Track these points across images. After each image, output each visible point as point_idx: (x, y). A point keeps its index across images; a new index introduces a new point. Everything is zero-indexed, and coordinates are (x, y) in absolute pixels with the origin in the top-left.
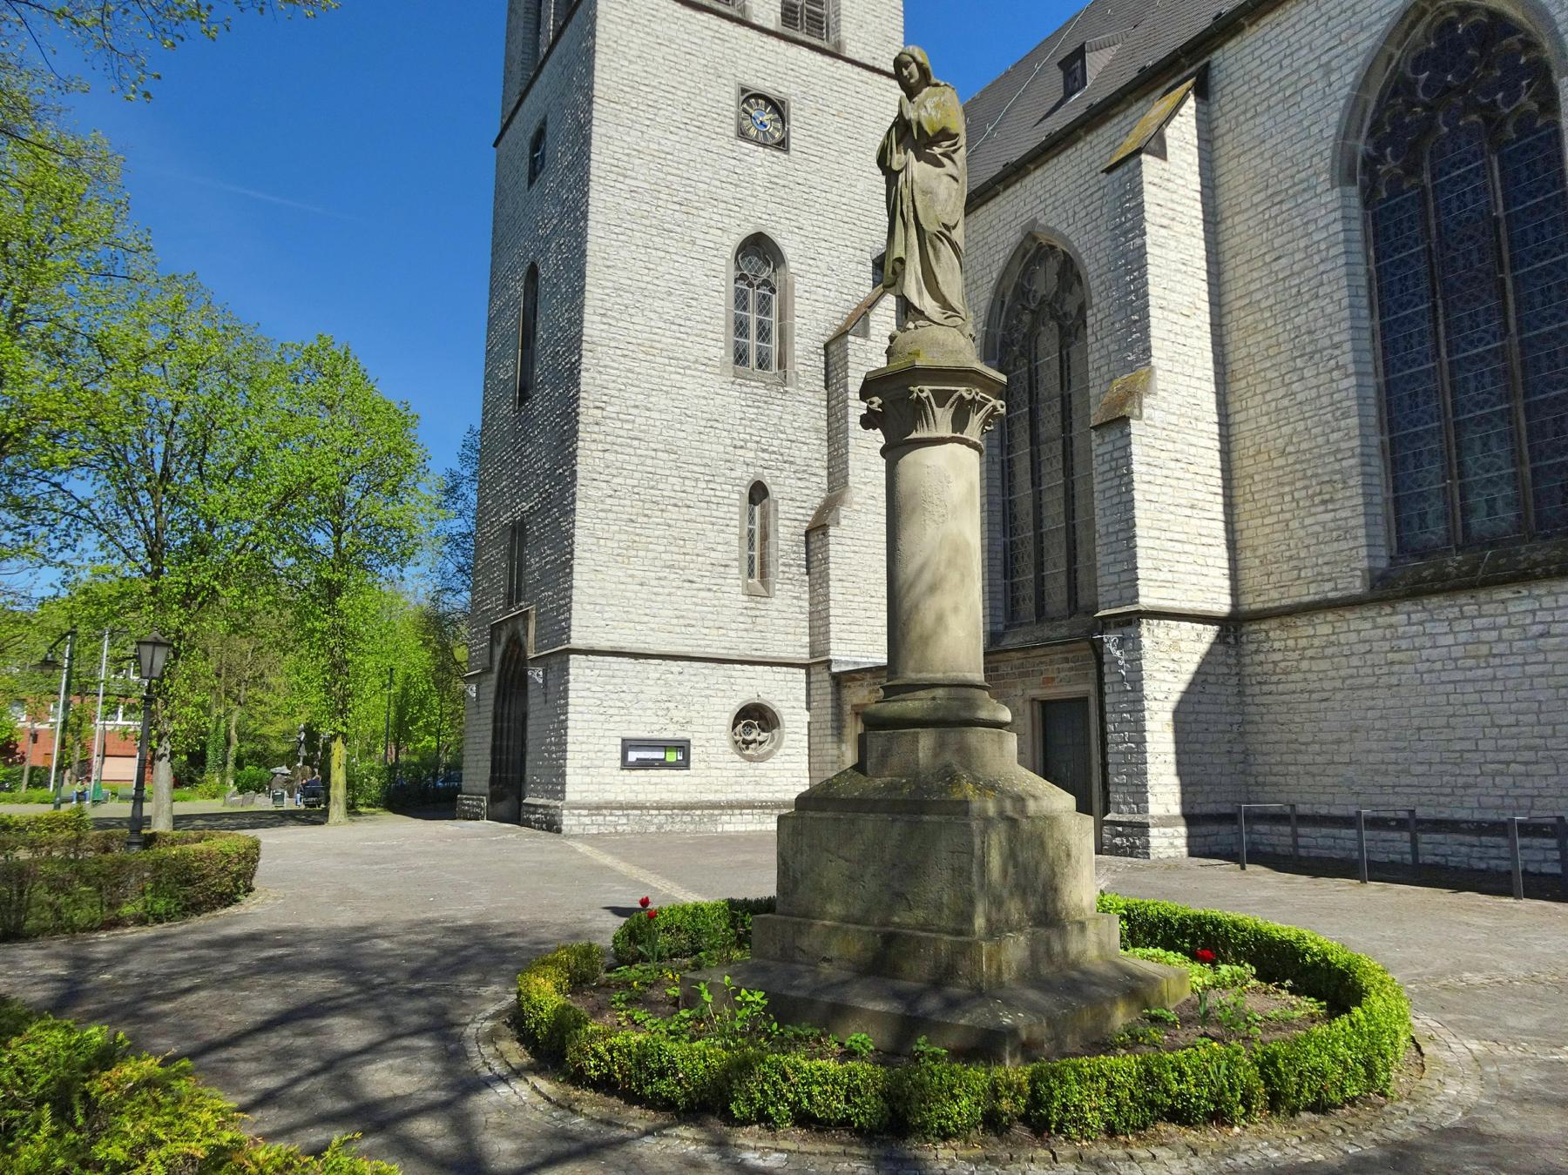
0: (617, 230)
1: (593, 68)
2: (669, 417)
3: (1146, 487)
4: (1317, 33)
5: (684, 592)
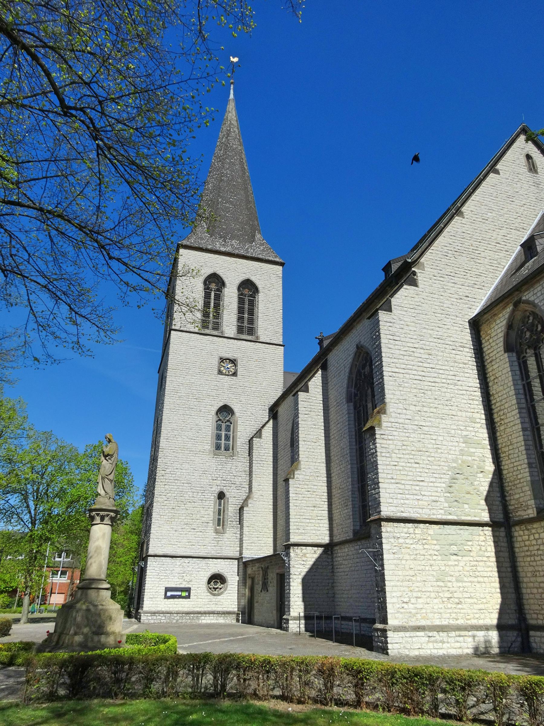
0: (174, 410)
2: (189, 471)
3: (295, 501)
5: (191, 533)
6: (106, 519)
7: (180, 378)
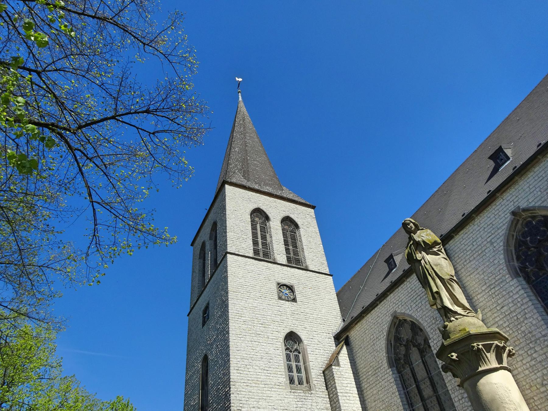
0: (240, 336)
1: (227, 282)
4: (482, 233)
7: (243, 301)
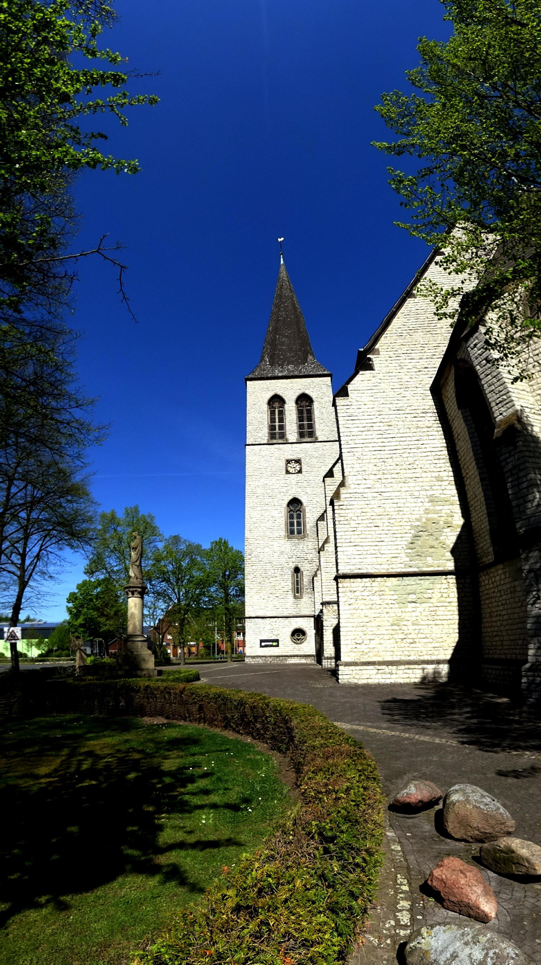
6: (136, 593)
